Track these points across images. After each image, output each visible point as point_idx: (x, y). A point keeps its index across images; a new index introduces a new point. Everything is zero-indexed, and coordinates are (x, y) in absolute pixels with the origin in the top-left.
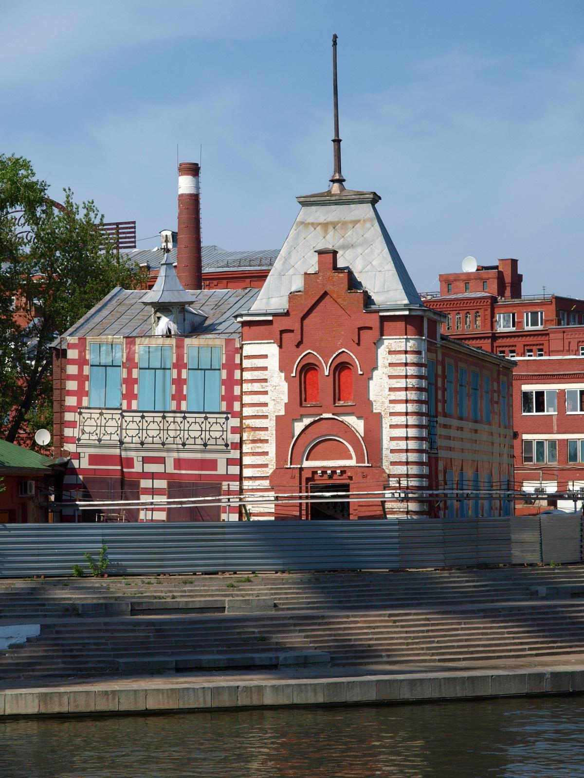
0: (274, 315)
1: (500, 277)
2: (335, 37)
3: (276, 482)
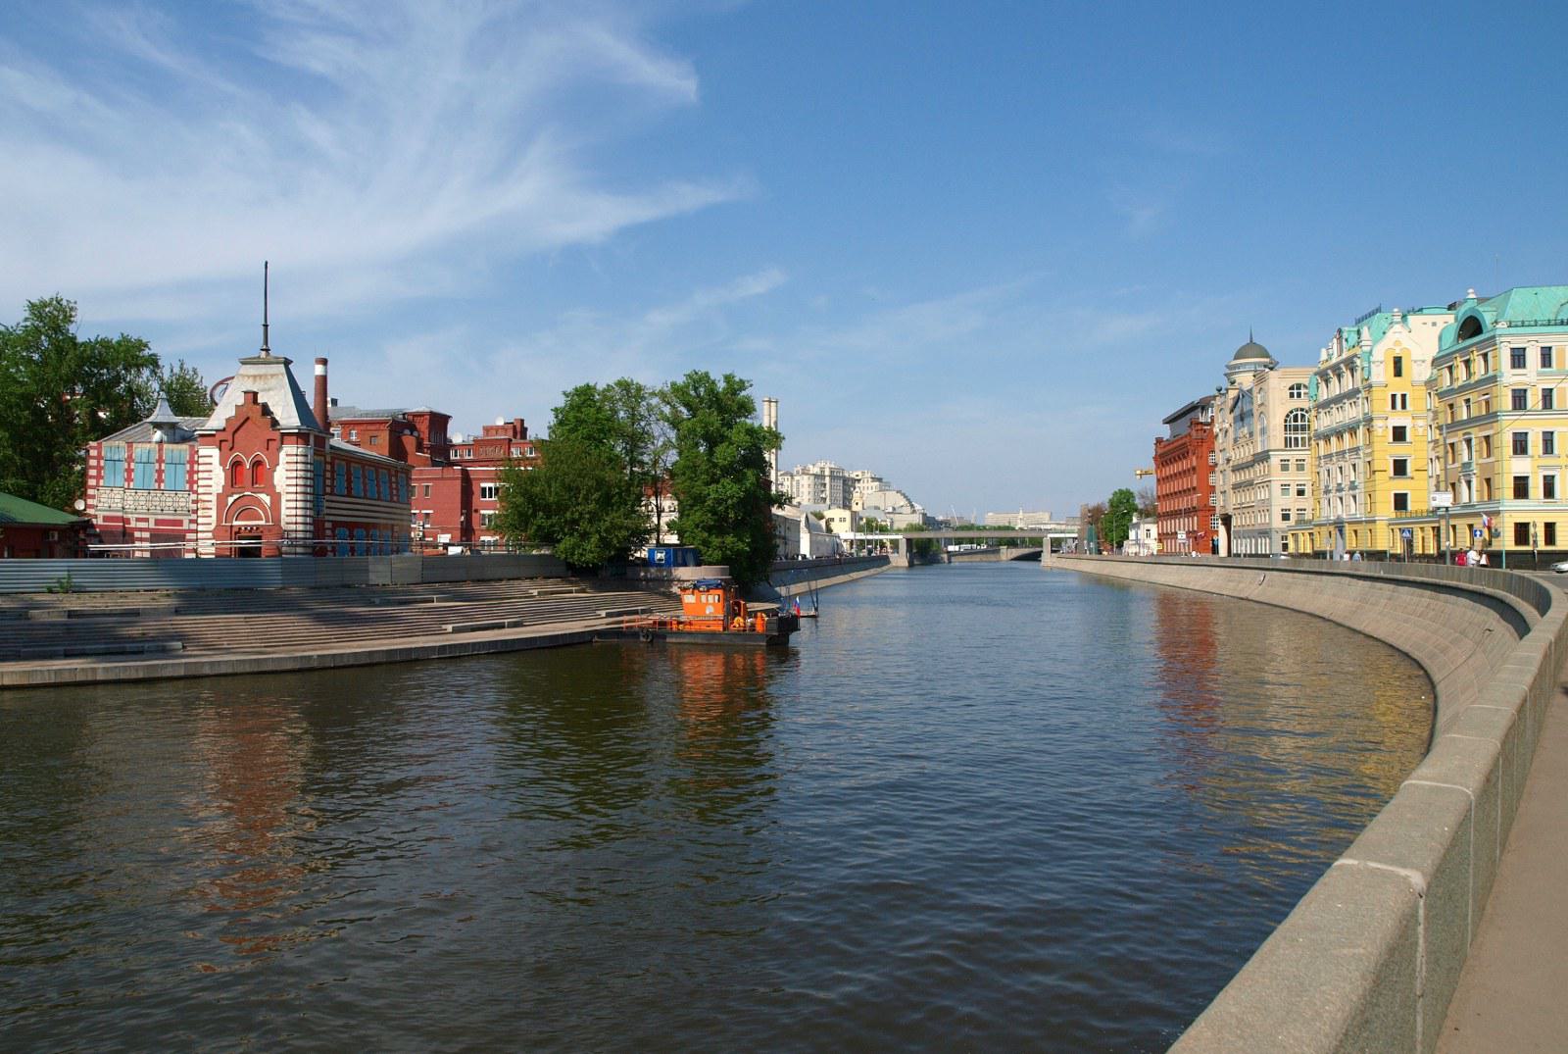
0: (216, 430)
1: (515, 427)
2: (266, 263)
3: (216, 534)
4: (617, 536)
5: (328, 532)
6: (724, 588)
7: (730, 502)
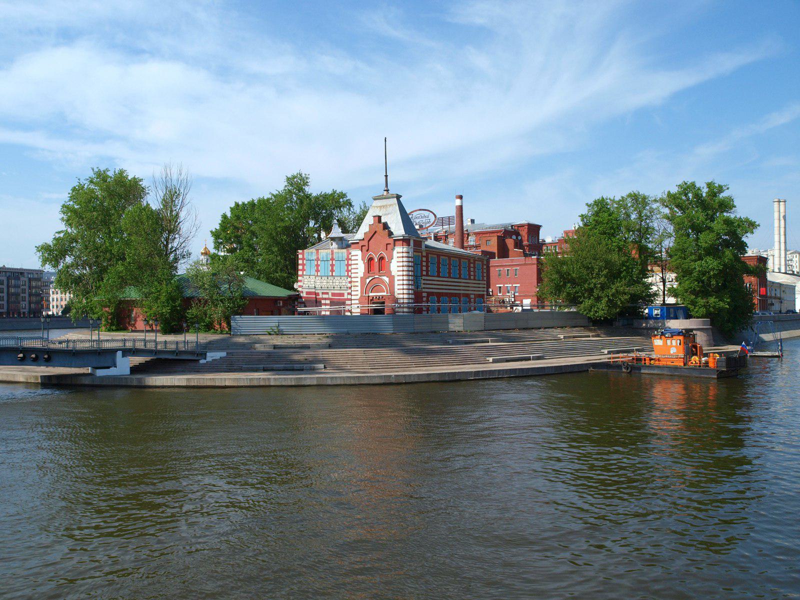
0: (360, 240)
4: (620, 299)
5: (424, 299)
6: (684, 335)
7: (712, 273)
